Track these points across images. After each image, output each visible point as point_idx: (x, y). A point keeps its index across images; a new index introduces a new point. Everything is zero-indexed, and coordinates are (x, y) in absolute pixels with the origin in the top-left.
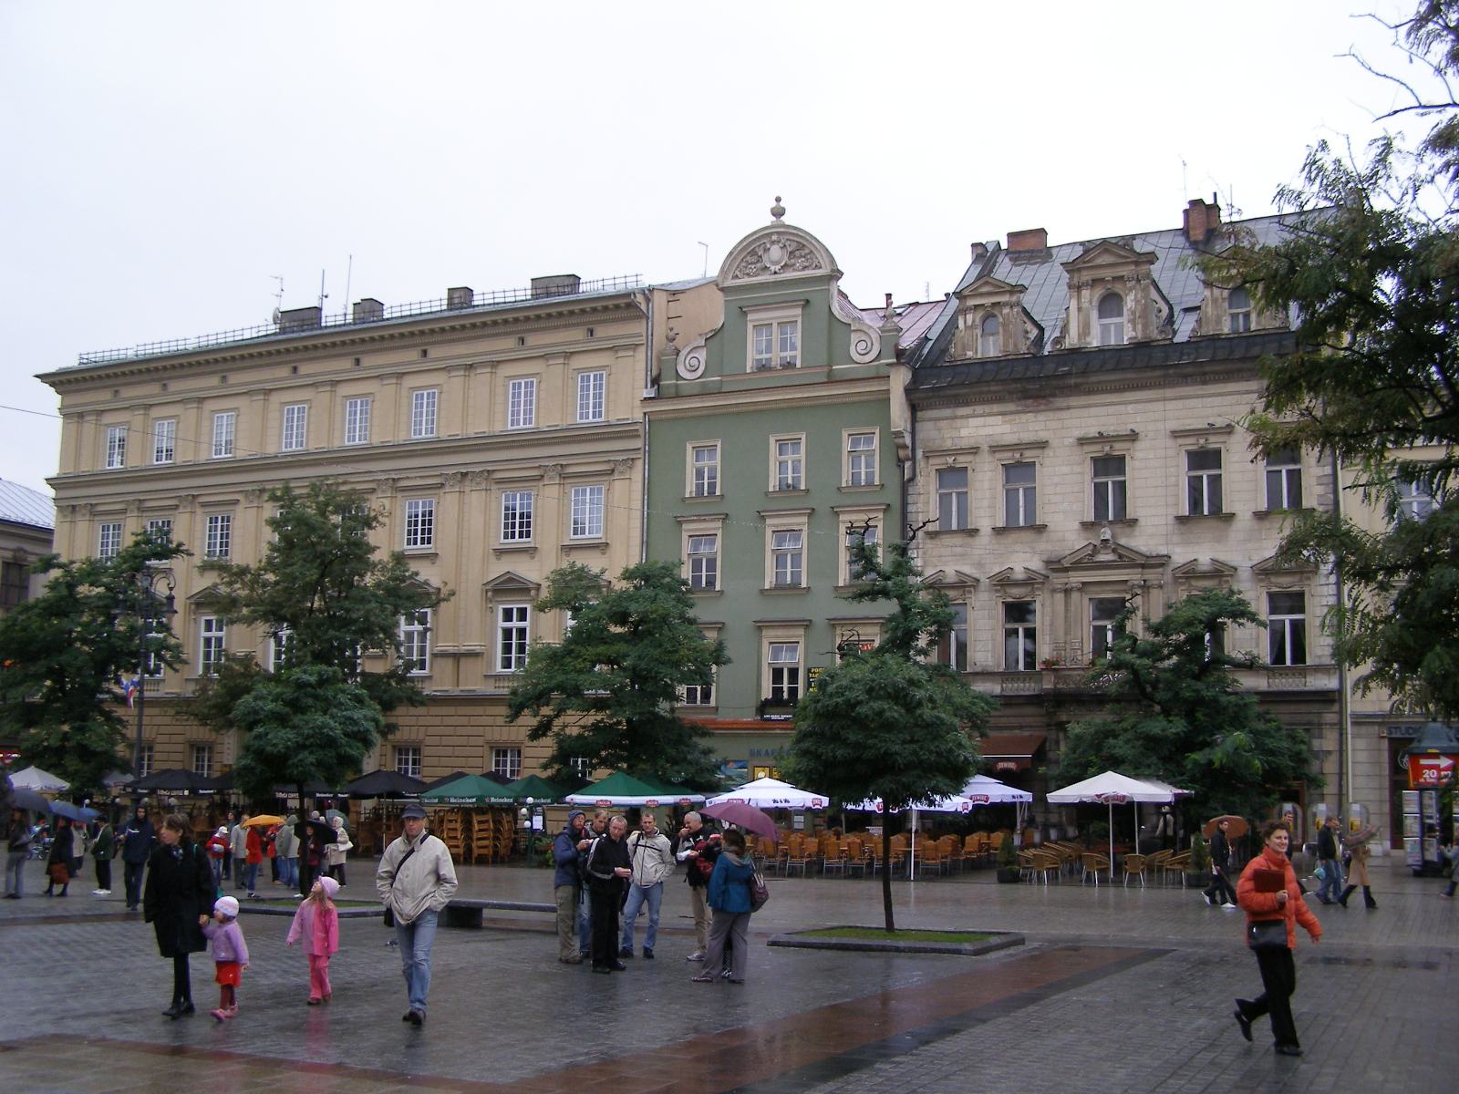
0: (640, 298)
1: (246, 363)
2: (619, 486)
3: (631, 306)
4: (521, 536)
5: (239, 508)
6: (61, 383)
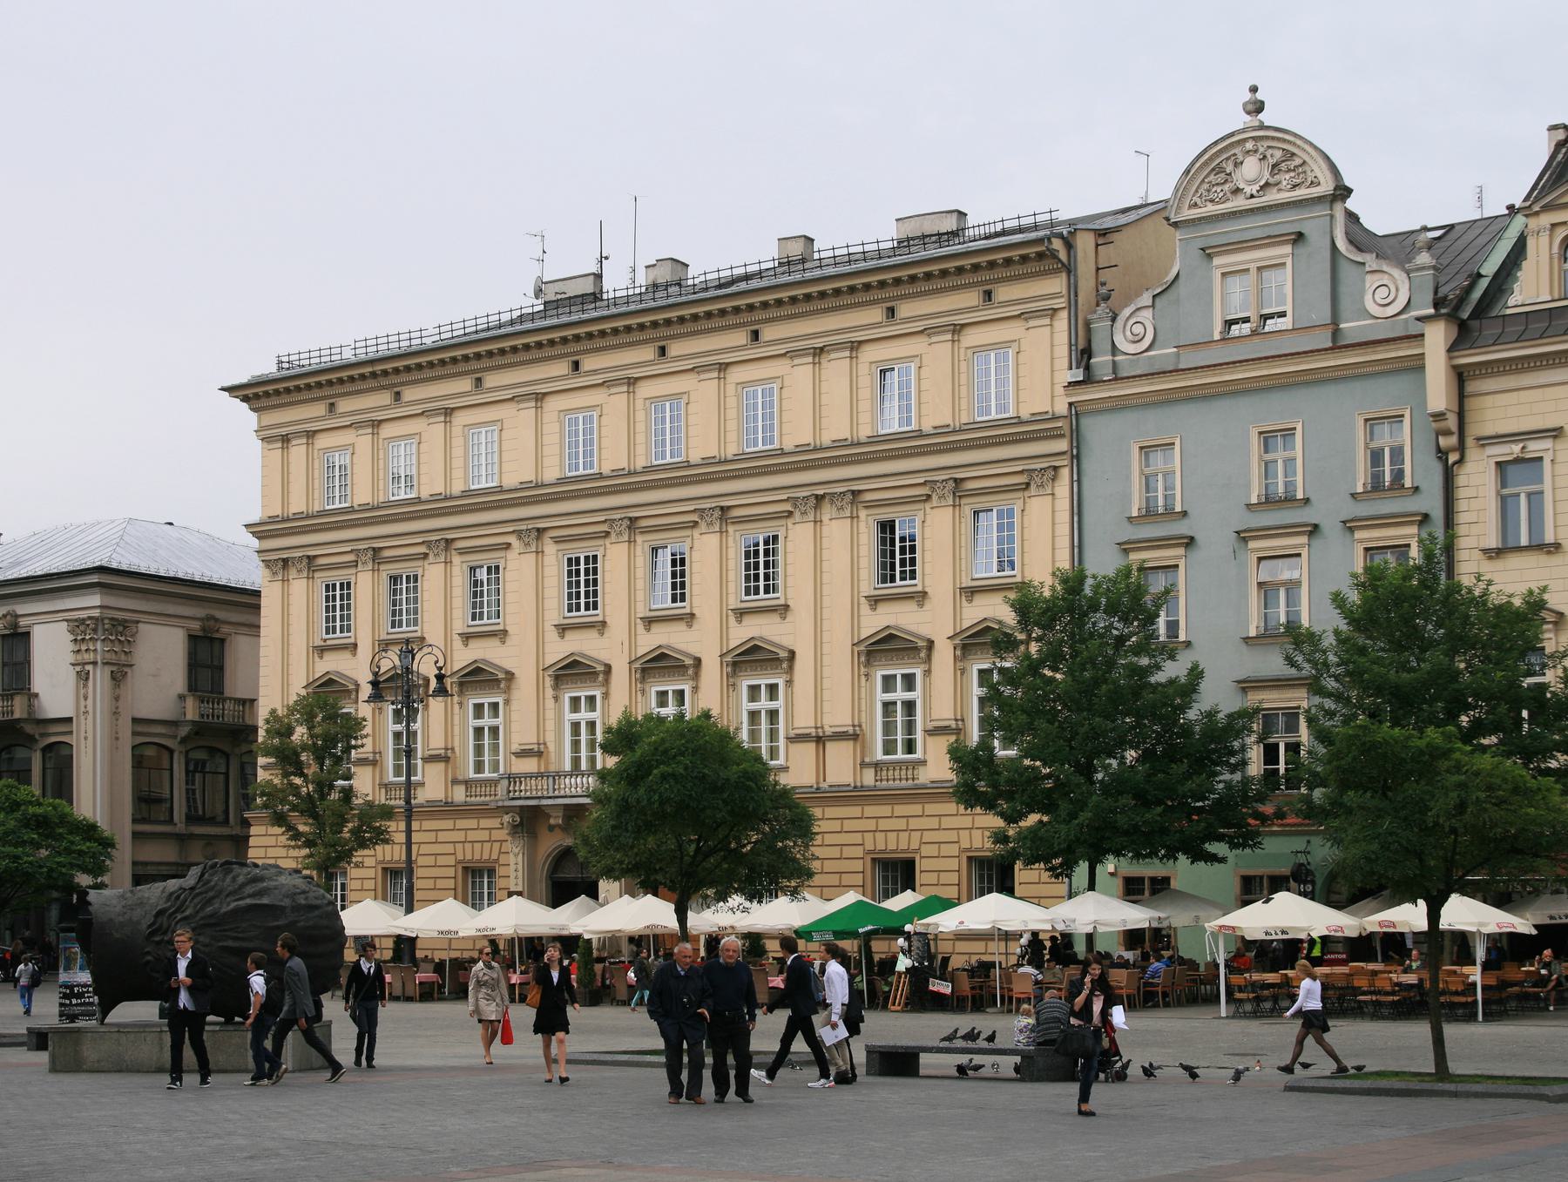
0: (1057, 244)
1: (783, 311)
3: (1046, 256)
4: (587, 608)
5: (512, 555)
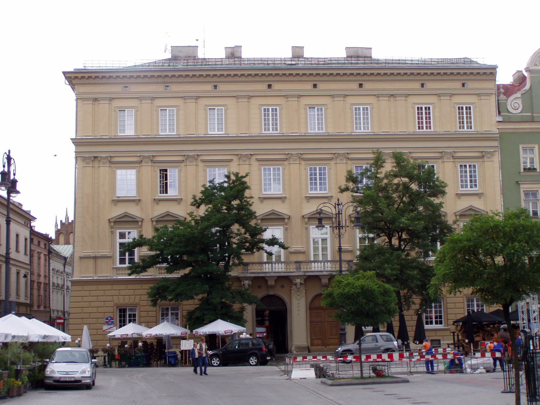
2: (487, 164)
6: (70, 77)
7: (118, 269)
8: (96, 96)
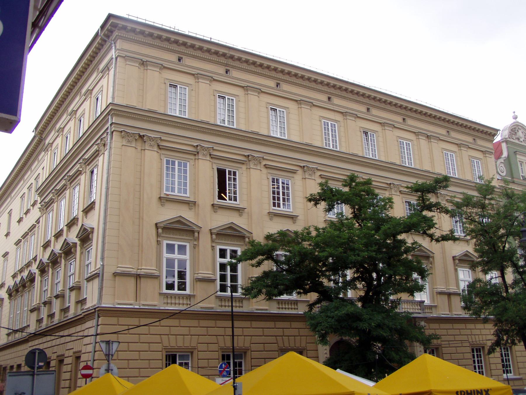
7: (166, 295)
8: (145, 59)
